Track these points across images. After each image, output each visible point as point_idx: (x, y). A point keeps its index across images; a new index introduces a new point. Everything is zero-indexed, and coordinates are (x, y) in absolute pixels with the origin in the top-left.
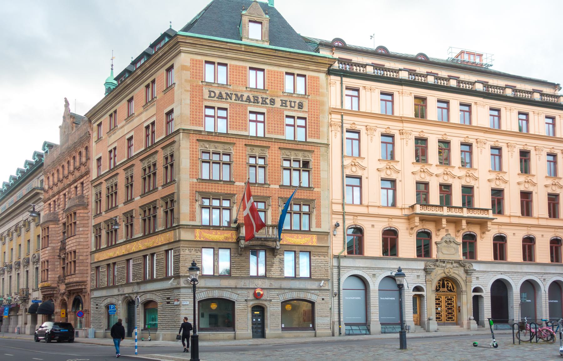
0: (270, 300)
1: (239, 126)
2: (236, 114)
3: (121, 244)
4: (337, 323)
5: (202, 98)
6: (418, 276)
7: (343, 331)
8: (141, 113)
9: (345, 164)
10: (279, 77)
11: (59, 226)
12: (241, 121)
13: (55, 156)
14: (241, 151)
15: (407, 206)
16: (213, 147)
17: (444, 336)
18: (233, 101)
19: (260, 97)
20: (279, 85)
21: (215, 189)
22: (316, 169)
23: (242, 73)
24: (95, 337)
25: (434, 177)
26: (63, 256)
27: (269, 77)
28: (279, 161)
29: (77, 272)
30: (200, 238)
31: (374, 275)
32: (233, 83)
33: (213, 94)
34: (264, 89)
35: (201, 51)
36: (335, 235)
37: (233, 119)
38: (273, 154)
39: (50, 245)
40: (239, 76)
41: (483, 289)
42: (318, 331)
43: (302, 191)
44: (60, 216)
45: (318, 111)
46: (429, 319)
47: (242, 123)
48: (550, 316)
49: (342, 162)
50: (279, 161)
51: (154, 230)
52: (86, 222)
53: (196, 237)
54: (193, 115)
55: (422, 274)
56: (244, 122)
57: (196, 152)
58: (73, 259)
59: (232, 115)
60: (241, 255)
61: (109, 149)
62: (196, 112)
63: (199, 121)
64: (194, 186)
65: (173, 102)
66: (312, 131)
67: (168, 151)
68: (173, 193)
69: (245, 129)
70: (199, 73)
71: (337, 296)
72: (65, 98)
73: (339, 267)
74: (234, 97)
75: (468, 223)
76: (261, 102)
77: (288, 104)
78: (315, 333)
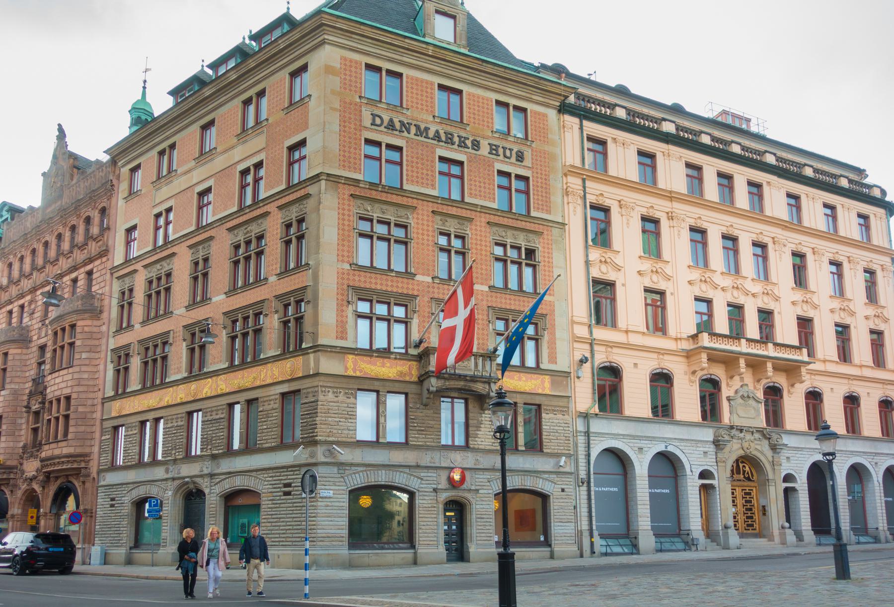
0: (477, 490)
1: (423, 178)
2: (417, 158)
3: (176, 383)
4: (586, 534)
5: (360, 125)
6: (705, 453)
7: (597, 548)
8: (232, 147)
9: (590, 258)
10: (486, 106)
11: (29, 351)
12: (425, 172)
13: (28, 225)
14: (425, 222)
15: (685, 336)
16: (378, 211)
17: (788, 555)
18: (412, 135)
19: (456, 135)
20: (486, 119)
21: (381, 284)
22: (546, 264)
23: (427, 92)
24: (105, 564)
25: (719, 291)
26: (35, 407)
27: (469, 104)
28: (488, 244)
29: (70, 436)
30: (355, 372)
31: (641, 449)
32: (412, 107)
33: (378, 121)
34: (462, 121)
35: (360, 46)
36: (578, 378)
37: (412, 167)
38: (479, 233)
39: (7, 386)
40: (422, 95)
41: (797, 477)
42: (557, 549)
43: (526, 299)
44: (33, 333)
45: (547, 169)
46: (726, 527)
47: (427, 175)
48: (888, 524)
49: (587, 256)
50: (488, 244)
51: (125, 389)
52: (96, 342)
53: (346, 369)
54: (344, 151)
55: (711, 449)
56: (429, 173)
57: (349, 216)
58: (62, 412)
59: (409, 158)
60: (426, 405)
61: (156, 211)
62: (350, 147)
63: (355, 163)
64: (346, 276)
65: (306, 127)
66: (538, 199)
67: (293, 213)
68: (305, 288)
69: (432, 185)
70: (356, 82)
71: (585, 484)
72: (59, 125)
73: (587, 434)
74: (413, 130)
75: (775, 368)
76: (457, 143)
77: (501, 151)
78: (415, 553)
